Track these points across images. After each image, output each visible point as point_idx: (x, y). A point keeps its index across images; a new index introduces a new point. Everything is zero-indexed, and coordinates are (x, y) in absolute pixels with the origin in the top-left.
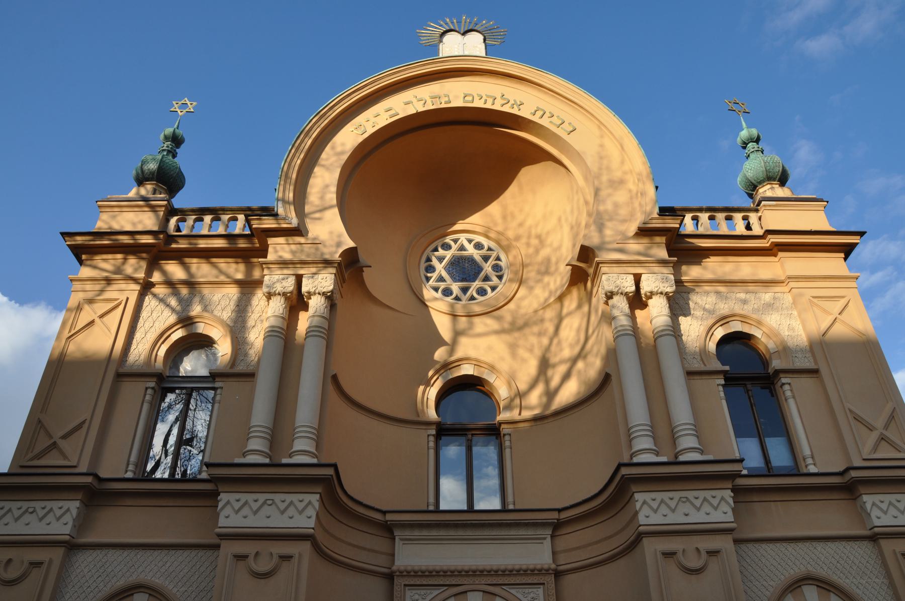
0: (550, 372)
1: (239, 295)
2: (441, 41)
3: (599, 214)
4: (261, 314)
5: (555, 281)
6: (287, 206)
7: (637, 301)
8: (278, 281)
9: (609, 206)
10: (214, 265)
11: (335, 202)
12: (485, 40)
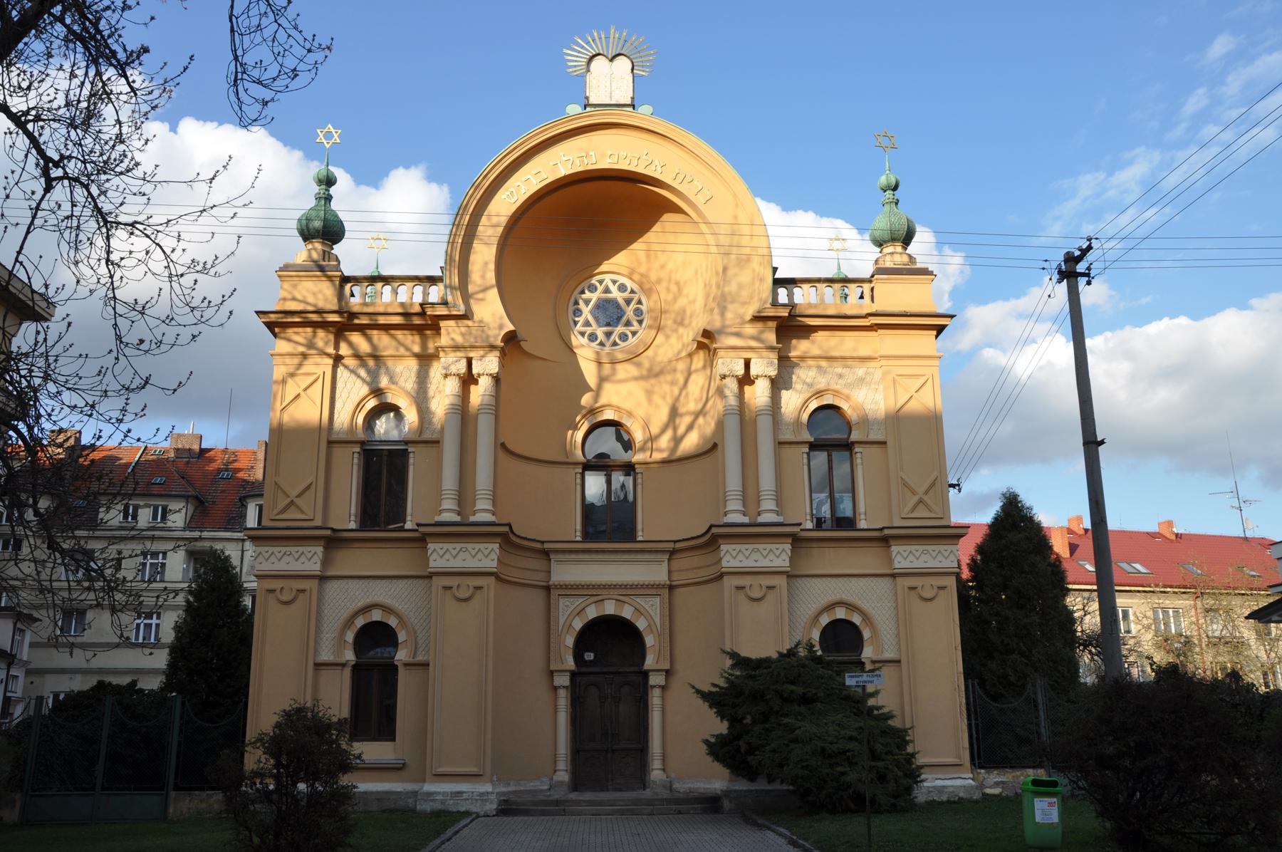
0: (678, 421)
1: (418, 367)
3: (723, 296)
7: (746, 379)
8: (453, 363)
9: (732, 288)
10: (393, 337)
11: (494, 282)
12: (633, 69)
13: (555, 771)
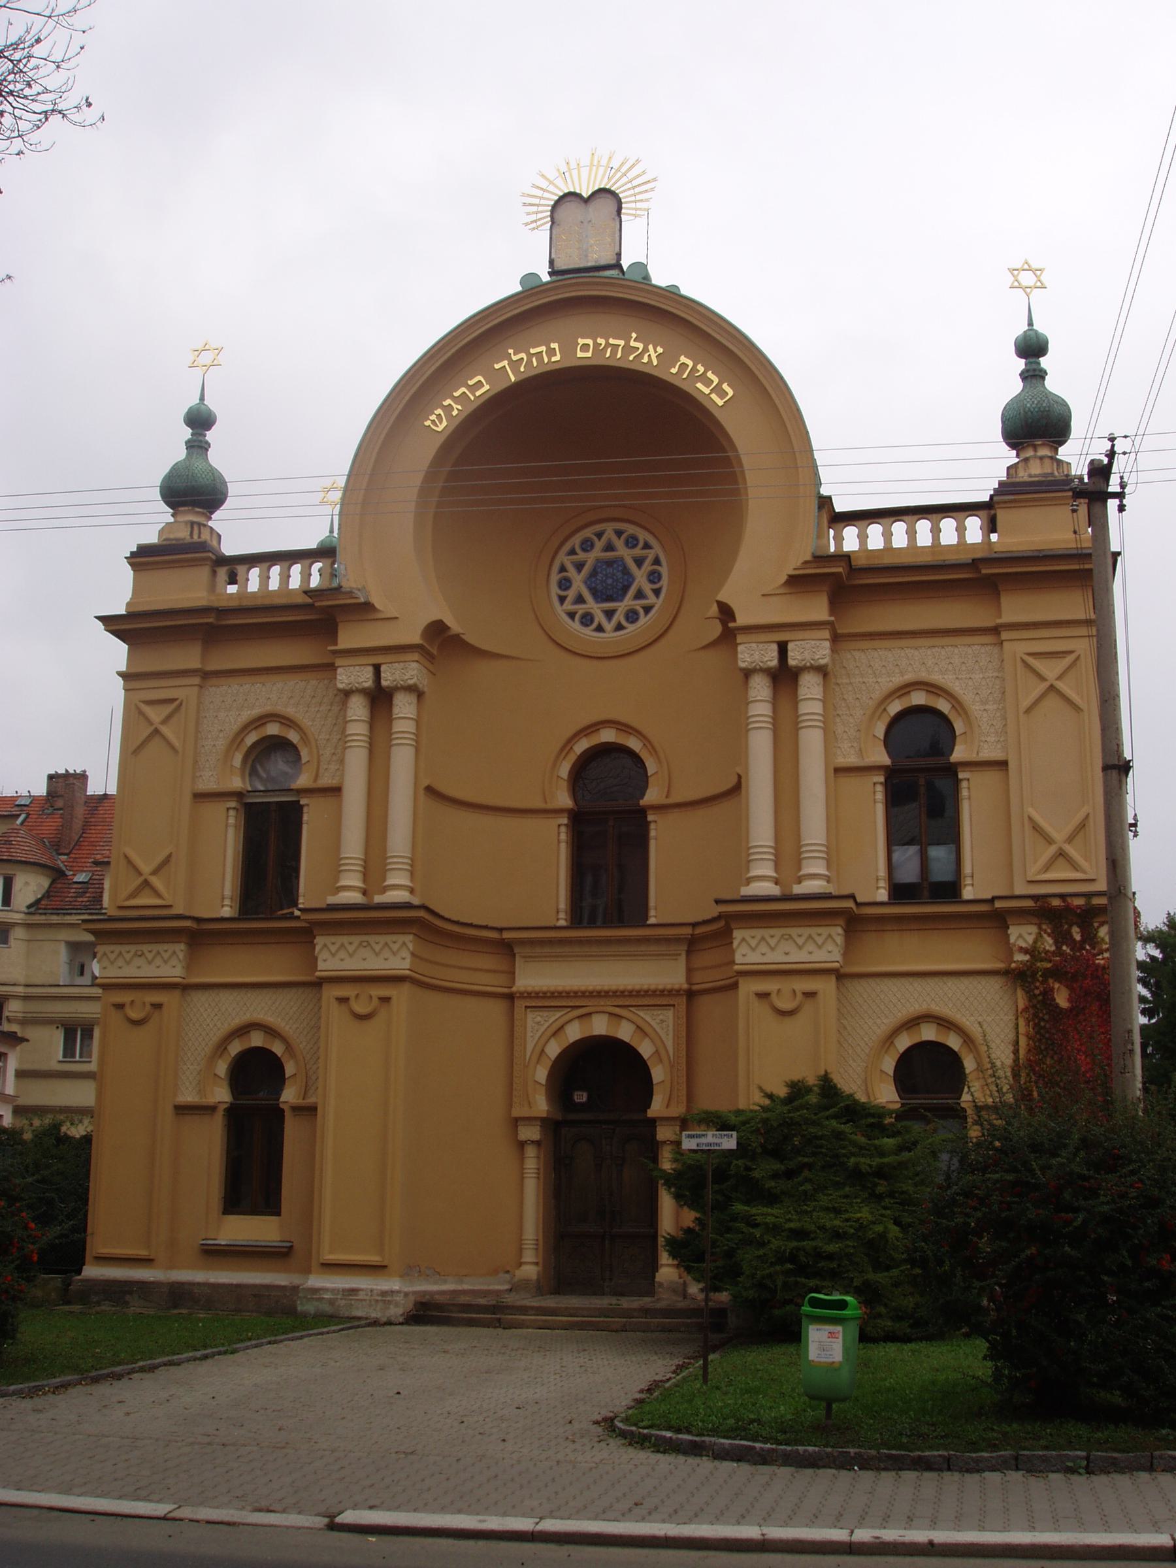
13: (521, 1264)
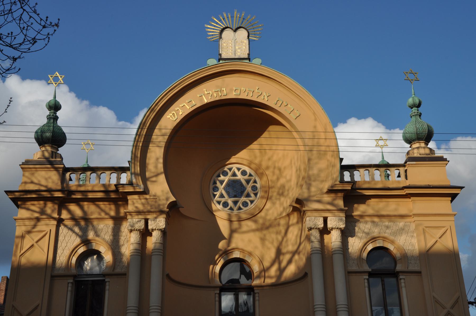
0: (281, 257)
2: (221, 37)
3: (309, 177)
4: (126, 237)
5: (287, 202)
6: (137, 177)
7: (325, 231)
9: (315, 171)
11: (162, 170)
12: (248, 36)
